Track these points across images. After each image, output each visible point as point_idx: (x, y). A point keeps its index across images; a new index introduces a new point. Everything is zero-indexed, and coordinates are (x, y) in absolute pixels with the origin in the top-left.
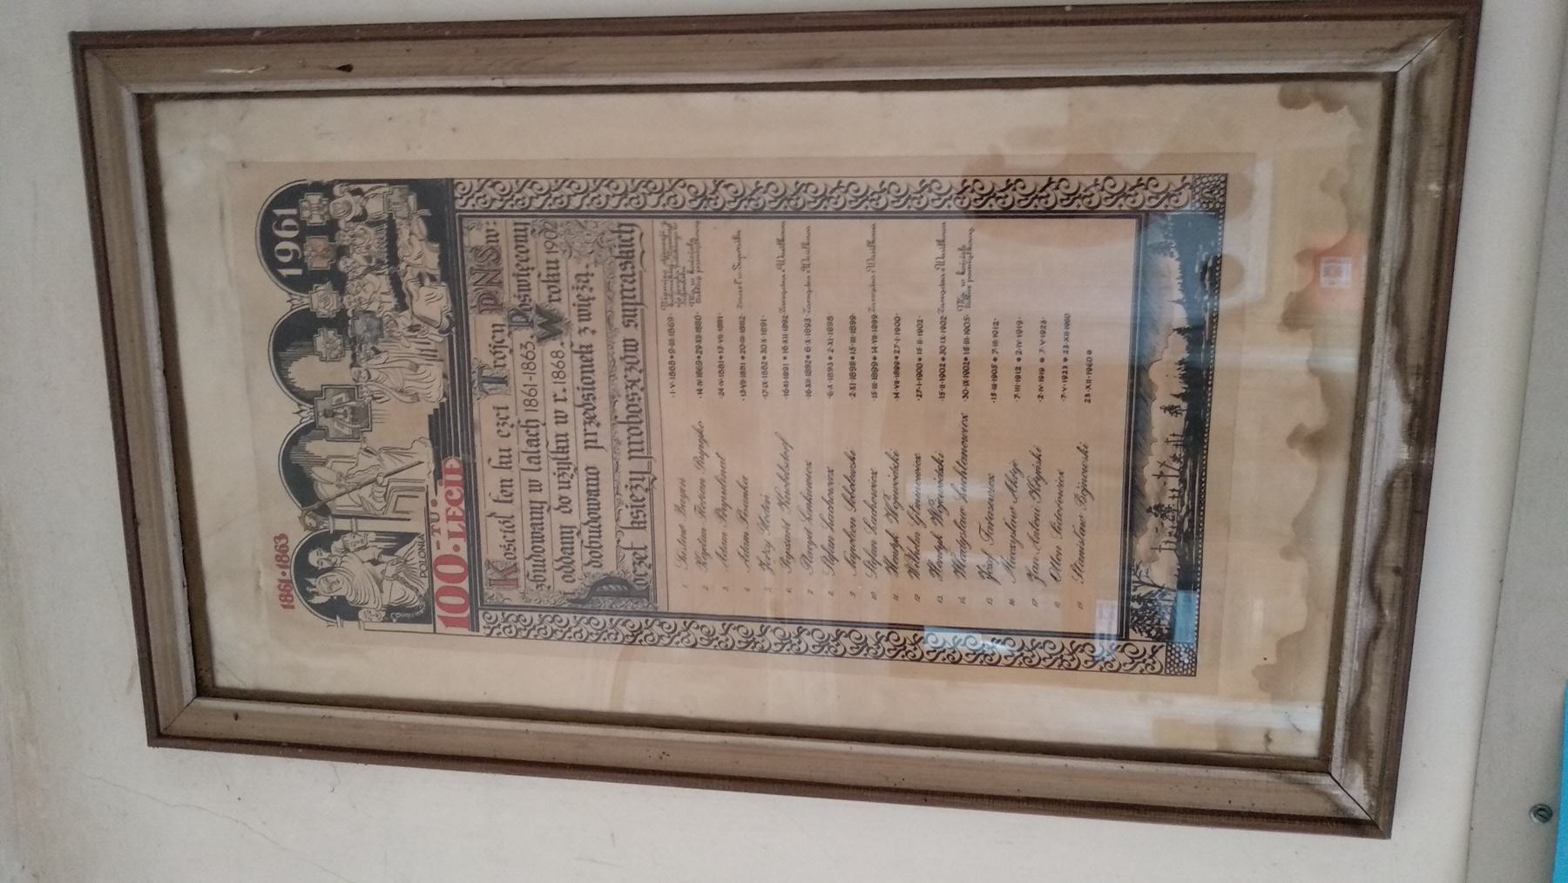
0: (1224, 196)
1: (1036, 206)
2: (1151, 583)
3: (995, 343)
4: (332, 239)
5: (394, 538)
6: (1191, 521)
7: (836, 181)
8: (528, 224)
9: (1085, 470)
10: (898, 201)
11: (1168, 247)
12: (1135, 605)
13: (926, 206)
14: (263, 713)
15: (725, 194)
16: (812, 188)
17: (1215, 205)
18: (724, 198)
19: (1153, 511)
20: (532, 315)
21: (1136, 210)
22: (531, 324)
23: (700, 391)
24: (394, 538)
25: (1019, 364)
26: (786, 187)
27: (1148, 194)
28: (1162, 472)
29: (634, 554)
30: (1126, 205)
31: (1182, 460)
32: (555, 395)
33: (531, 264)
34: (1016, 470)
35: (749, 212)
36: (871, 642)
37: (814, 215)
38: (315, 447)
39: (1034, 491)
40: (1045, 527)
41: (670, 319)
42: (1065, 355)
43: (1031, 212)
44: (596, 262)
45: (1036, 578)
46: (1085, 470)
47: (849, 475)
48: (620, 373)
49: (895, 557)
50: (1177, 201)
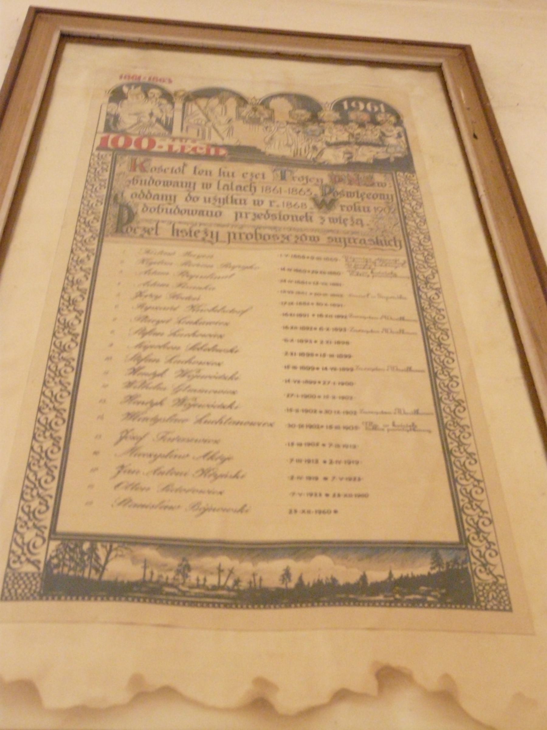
0: (492, 609)
1: (437, 368)
2: (110, 558)
3: (338, 446)
4: (368, 122)
5: (169, 123)
6: (174, 594)
7: (444, 307)
8: (393, 201)
9: (225, 510)
10: (445, 386)
11: (439, 565)
12: (86, 546)
13: (434, 354)
14: (45, 56)
15: (431, 293)
16: (445, 337)
17: (483, 601)
18: (425, 272)
19: (184, 563)
20: (331, 196)
21: (467, 540)
22: (324, 194)
23: (283, 269)
24: (169, 123)
25: (321, 461)
26: (444, 324)
27: (483, 549)
28: (223, 571)
29: (152, 229)
30: (470, 533)
31: (236, 588)
32: (274, 202)
33: (366, 199)
34: (223, 460)
35: (429, 347)
36: (65, 355)
37: (426, 338)
38: (232, 103)
39: (204, 472)
40: (167, 480)
41: (336, 260)
42: (331, 495)
43: (463, 527)
44: (372, 229)
45: (119, 472)
46: (225, 510)
47: (218, 348)
48: (294, 233)
49: (146, 374)
50: (480, 571)
